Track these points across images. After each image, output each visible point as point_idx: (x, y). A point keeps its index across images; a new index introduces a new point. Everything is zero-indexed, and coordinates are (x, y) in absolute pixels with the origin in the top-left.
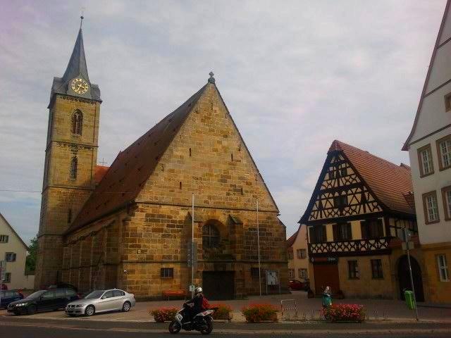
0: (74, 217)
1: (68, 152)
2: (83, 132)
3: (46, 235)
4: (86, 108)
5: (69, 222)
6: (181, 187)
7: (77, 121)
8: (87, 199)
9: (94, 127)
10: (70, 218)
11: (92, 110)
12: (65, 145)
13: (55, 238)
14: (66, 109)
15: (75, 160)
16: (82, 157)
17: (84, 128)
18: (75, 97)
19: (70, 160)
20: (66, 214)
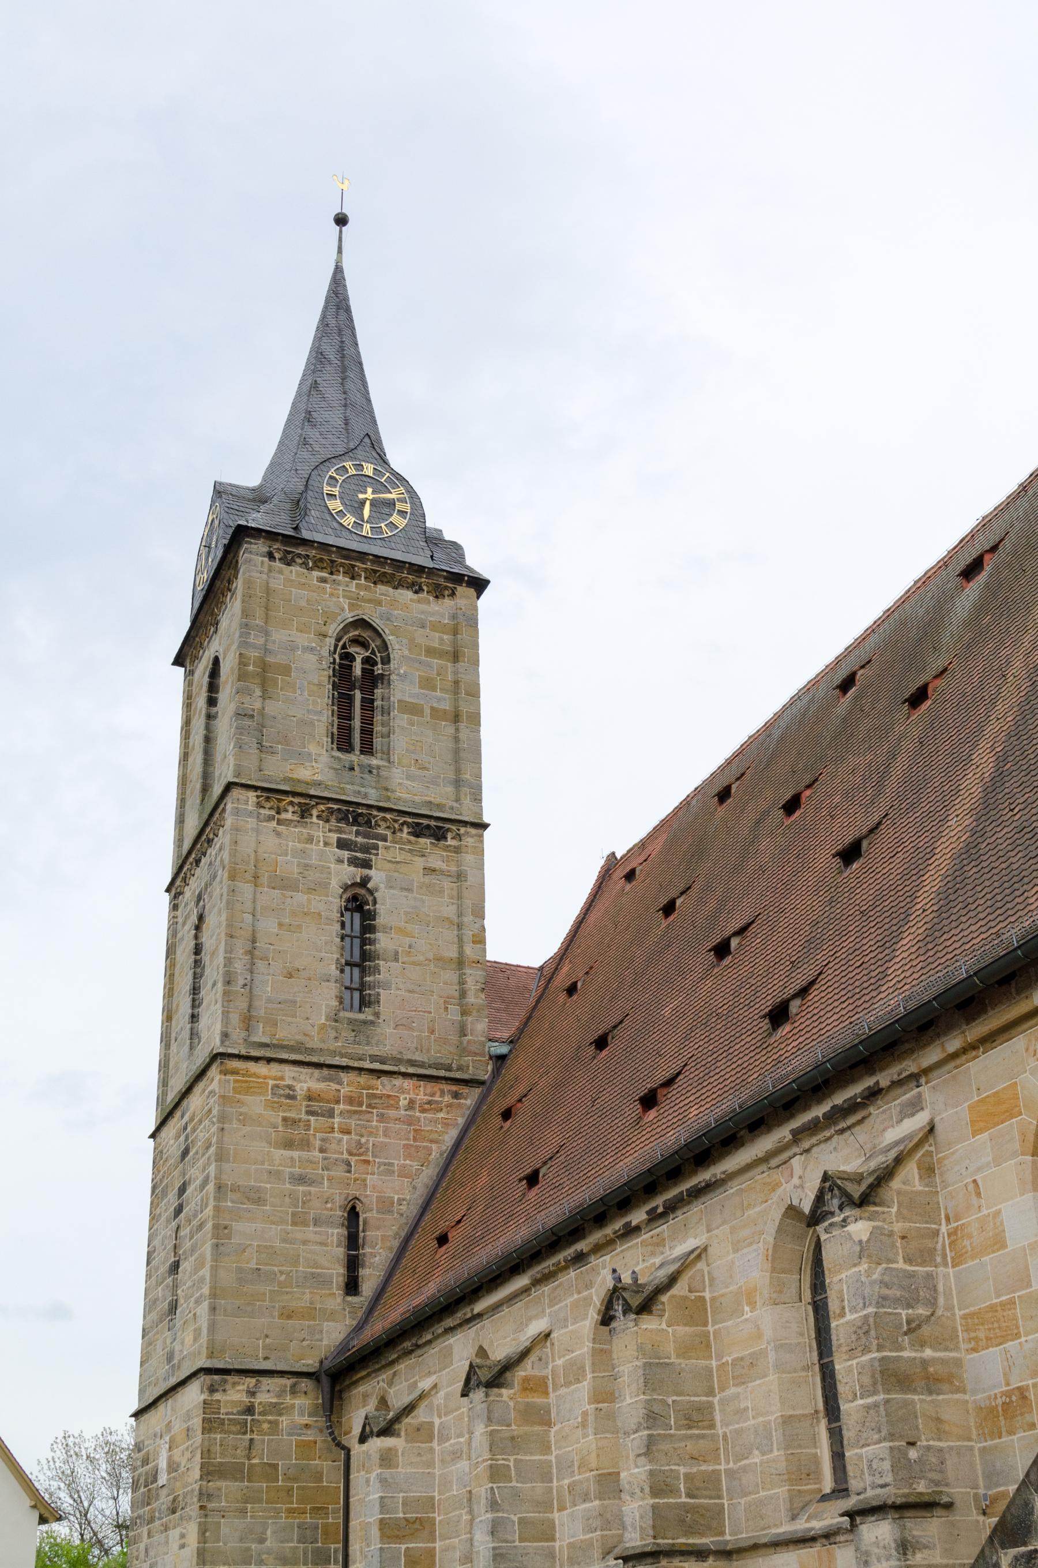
0: (377, 1257)
1: (316, 853)
2: (400, 743)
3: (217, 1374)
4: (401, 611)
5: (352, 1286)
6: (353, 1214)
7: (358, 679)
8: (453, 1134)
9: (456, 718)
10: (353, 1264)
11: (435, 627)
12: (304, 812)
13: (268, 1392)
14: (301, 614)
15: (359, 904)
16: (399, 875)
17: (400, 720)
18: (345, 552)
19: (333, 902)
20: (337, 1233)
